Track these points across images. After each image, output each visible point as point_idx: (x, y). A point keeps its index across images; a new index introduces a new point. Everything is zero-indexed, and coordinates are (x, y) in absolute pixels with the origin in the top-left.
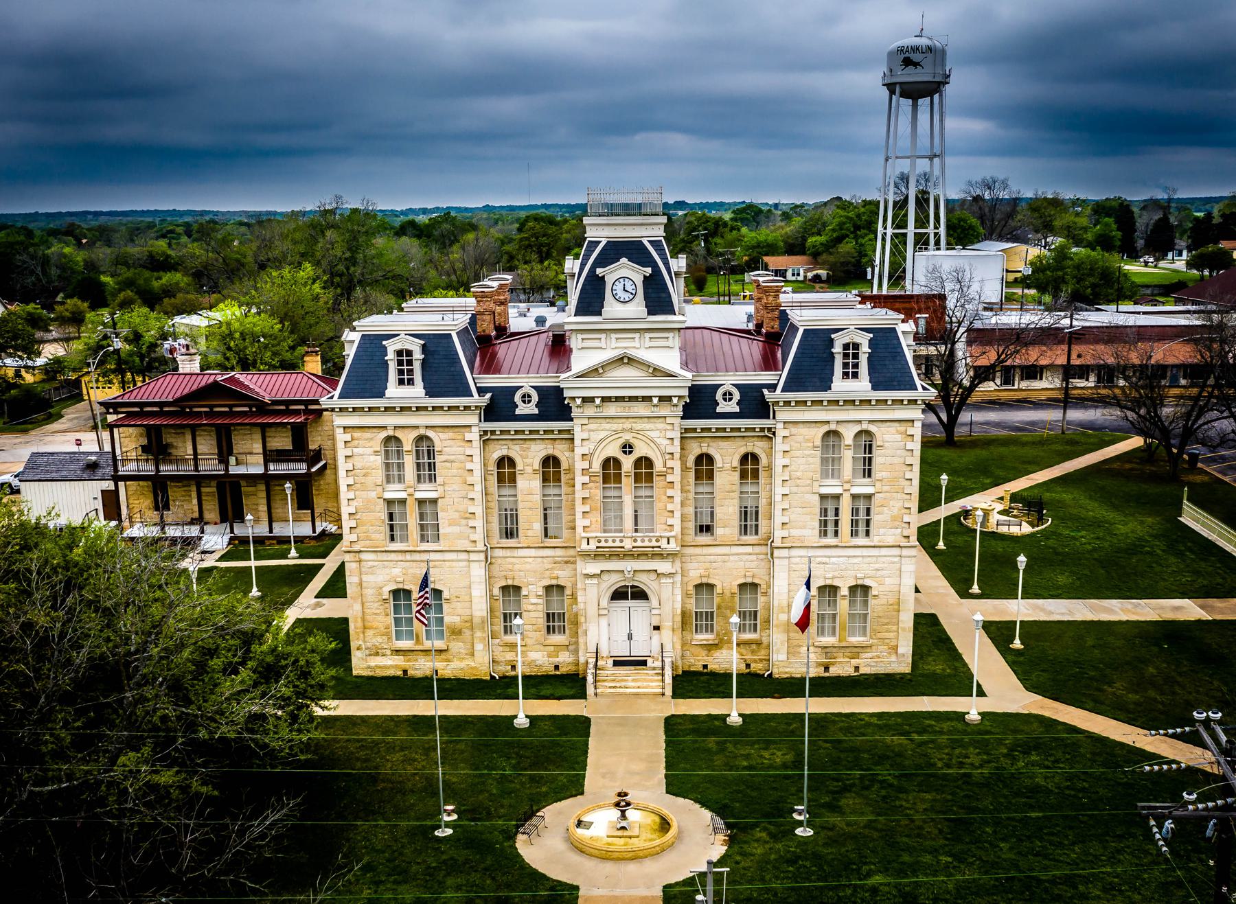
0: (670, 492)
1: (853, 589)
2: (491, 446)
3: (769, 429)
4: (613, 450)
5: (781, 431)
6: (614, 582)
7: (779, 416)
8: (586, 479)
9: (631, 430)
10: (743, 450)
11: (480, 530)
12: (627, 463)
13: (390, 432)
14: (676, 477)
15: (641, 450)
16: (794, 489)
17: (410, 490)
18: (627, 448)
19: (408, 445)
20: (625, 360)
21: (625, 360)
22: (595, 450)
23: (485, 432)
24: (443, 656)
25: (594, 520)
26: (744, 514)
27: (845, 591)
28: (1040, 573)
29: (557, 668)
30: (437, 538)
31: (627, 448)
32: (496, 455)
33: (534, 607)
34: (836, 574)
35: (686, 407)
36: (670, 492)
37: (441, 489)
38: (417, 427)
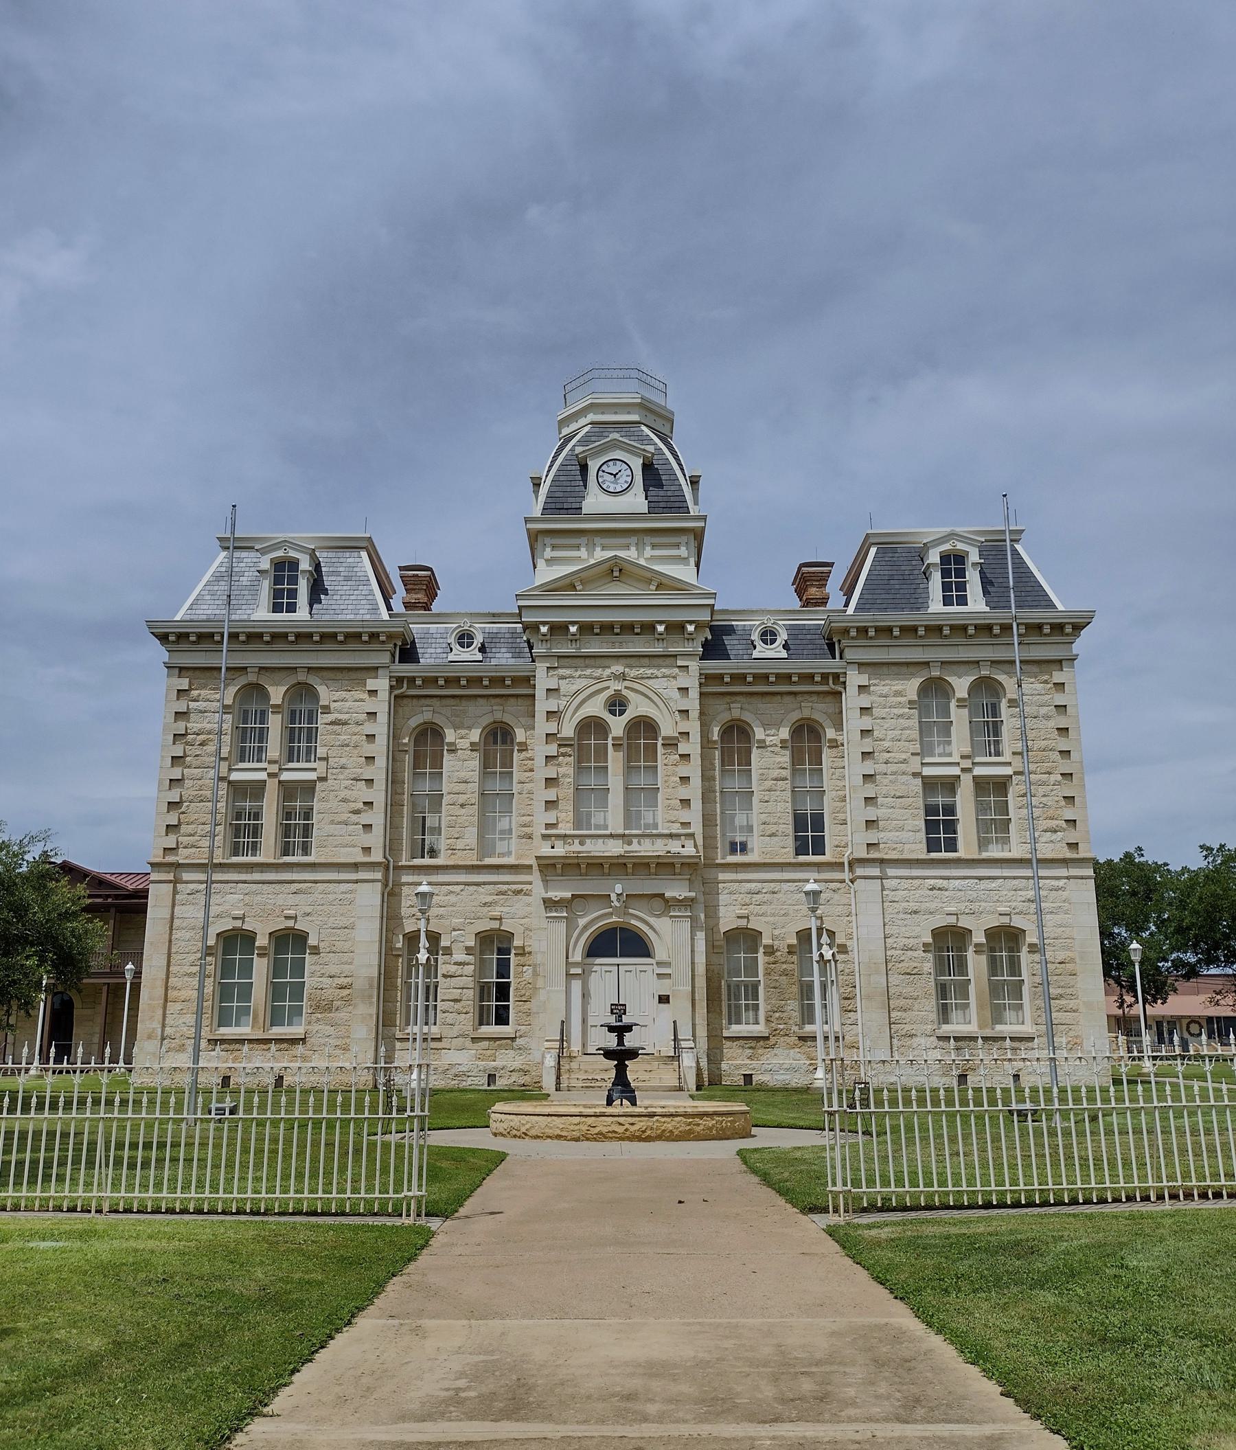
0: (683, 770)
1: (993, 934)
2: (408, 705)
3: (836, 676)
4: (595, 707)
5: (855, 678)
6: (591, 921)
7: (850, 654)
8: (552, 749)
9: (623, 677)
10: (795, 716)
11: (378, 830)
12: (617, 726)
13: (252, 678)
14: (692, 747)
15: (638, 707)
16: (881, 768)
17: (274, 768)
18: (617, 705)
19: (277, 694)
20: (616, 571)
21: (616, 571)
22: (567, 708)
23: (400, 680)
24: (299, 1050)
25: (562, 816)
26: (800, 822)
27: (979, 938)
28: (423, 1404)
29: (491, 1078)
30: (306, 850)
31: (617, 705)
32: (414, 722)
33: (459, 978)
34: (962, 907)
35: (705, 645)
36: (683, 770)
37: (320, 766)
38: (294, 669)
